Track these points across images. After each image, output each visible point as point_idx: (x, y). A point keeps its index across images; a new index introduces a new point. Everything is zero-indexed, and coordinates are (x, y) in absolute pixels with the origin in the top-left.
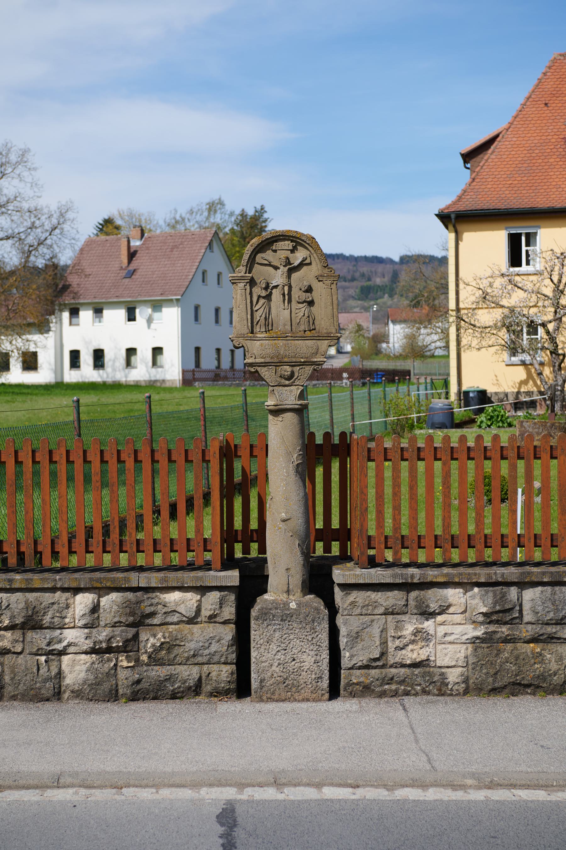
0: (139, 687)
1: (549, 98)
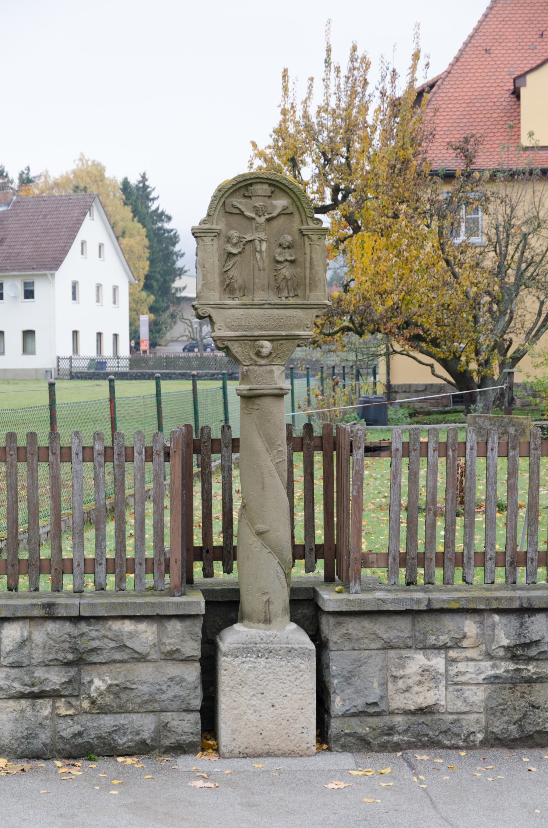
0: (80, 741)
1: (491, 44)
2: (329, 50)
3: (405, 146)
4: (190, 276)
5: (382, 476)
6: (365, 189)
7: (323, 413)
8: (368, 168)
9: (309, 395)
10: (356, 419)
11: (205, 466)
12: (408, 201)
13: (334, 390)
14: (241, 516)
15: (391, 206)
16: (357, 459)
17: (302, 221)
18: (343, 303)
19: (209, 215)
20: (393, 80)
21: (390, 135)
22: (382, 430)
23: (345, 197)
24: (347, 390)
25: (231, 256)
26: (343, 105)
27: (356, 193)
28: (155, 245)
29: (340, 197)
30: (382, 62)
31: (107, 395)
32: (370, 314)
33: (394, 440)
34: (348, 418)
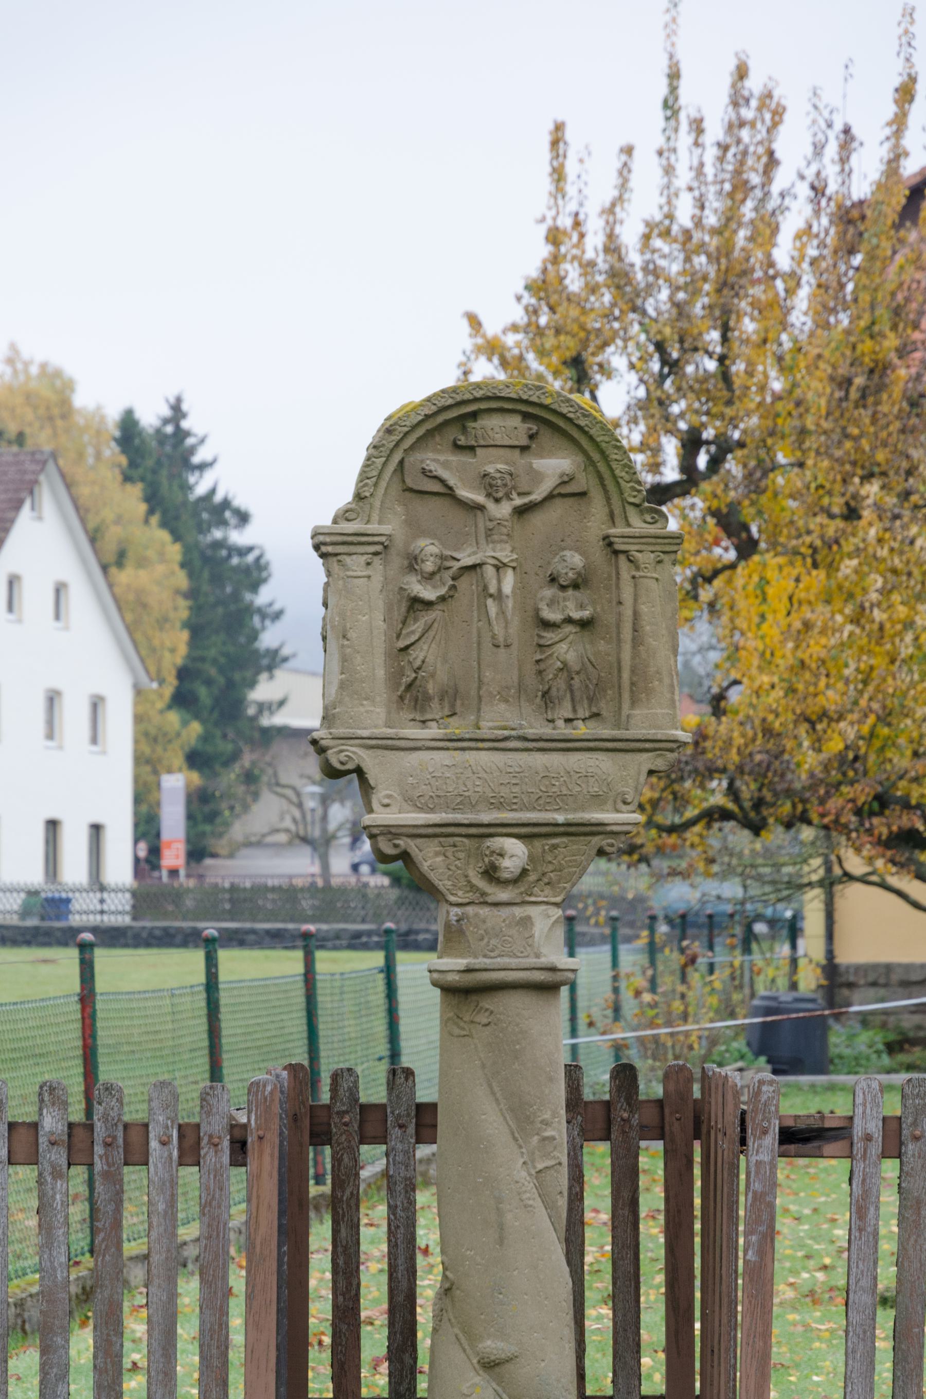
2: (674, 76)
3: (876, 328)
4: (296, 671)
5: (815, 1210)
6: (769, 441)
7: (656, 1039)
8: (777, 385)
9: (616, 990)
10: (742, 1057)
11: (346, 1175)
12: (884, 474)
13: (684, 979)
14: (439, 1316)
15: (838, 487)
16: (759, 1163)
17: (612, 515)
18: (708, 744)
19: (359, 497)
20: (844, 154)
21: (836, 298)
22: (813, 1086)
23: (715, 463)
24: (719, 979)
25: (417, 606)
26: (711, 220)
27: (745, 451)
28: (206, 588)
29: (702, 461)
30: (815, 107)
31: (75, 985)
32: (782, 775)
33: (859, 1110)
34: (721, 1054)
